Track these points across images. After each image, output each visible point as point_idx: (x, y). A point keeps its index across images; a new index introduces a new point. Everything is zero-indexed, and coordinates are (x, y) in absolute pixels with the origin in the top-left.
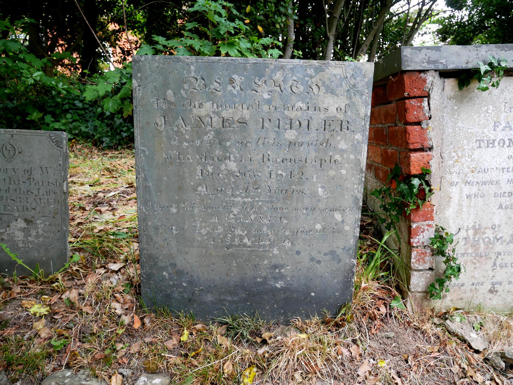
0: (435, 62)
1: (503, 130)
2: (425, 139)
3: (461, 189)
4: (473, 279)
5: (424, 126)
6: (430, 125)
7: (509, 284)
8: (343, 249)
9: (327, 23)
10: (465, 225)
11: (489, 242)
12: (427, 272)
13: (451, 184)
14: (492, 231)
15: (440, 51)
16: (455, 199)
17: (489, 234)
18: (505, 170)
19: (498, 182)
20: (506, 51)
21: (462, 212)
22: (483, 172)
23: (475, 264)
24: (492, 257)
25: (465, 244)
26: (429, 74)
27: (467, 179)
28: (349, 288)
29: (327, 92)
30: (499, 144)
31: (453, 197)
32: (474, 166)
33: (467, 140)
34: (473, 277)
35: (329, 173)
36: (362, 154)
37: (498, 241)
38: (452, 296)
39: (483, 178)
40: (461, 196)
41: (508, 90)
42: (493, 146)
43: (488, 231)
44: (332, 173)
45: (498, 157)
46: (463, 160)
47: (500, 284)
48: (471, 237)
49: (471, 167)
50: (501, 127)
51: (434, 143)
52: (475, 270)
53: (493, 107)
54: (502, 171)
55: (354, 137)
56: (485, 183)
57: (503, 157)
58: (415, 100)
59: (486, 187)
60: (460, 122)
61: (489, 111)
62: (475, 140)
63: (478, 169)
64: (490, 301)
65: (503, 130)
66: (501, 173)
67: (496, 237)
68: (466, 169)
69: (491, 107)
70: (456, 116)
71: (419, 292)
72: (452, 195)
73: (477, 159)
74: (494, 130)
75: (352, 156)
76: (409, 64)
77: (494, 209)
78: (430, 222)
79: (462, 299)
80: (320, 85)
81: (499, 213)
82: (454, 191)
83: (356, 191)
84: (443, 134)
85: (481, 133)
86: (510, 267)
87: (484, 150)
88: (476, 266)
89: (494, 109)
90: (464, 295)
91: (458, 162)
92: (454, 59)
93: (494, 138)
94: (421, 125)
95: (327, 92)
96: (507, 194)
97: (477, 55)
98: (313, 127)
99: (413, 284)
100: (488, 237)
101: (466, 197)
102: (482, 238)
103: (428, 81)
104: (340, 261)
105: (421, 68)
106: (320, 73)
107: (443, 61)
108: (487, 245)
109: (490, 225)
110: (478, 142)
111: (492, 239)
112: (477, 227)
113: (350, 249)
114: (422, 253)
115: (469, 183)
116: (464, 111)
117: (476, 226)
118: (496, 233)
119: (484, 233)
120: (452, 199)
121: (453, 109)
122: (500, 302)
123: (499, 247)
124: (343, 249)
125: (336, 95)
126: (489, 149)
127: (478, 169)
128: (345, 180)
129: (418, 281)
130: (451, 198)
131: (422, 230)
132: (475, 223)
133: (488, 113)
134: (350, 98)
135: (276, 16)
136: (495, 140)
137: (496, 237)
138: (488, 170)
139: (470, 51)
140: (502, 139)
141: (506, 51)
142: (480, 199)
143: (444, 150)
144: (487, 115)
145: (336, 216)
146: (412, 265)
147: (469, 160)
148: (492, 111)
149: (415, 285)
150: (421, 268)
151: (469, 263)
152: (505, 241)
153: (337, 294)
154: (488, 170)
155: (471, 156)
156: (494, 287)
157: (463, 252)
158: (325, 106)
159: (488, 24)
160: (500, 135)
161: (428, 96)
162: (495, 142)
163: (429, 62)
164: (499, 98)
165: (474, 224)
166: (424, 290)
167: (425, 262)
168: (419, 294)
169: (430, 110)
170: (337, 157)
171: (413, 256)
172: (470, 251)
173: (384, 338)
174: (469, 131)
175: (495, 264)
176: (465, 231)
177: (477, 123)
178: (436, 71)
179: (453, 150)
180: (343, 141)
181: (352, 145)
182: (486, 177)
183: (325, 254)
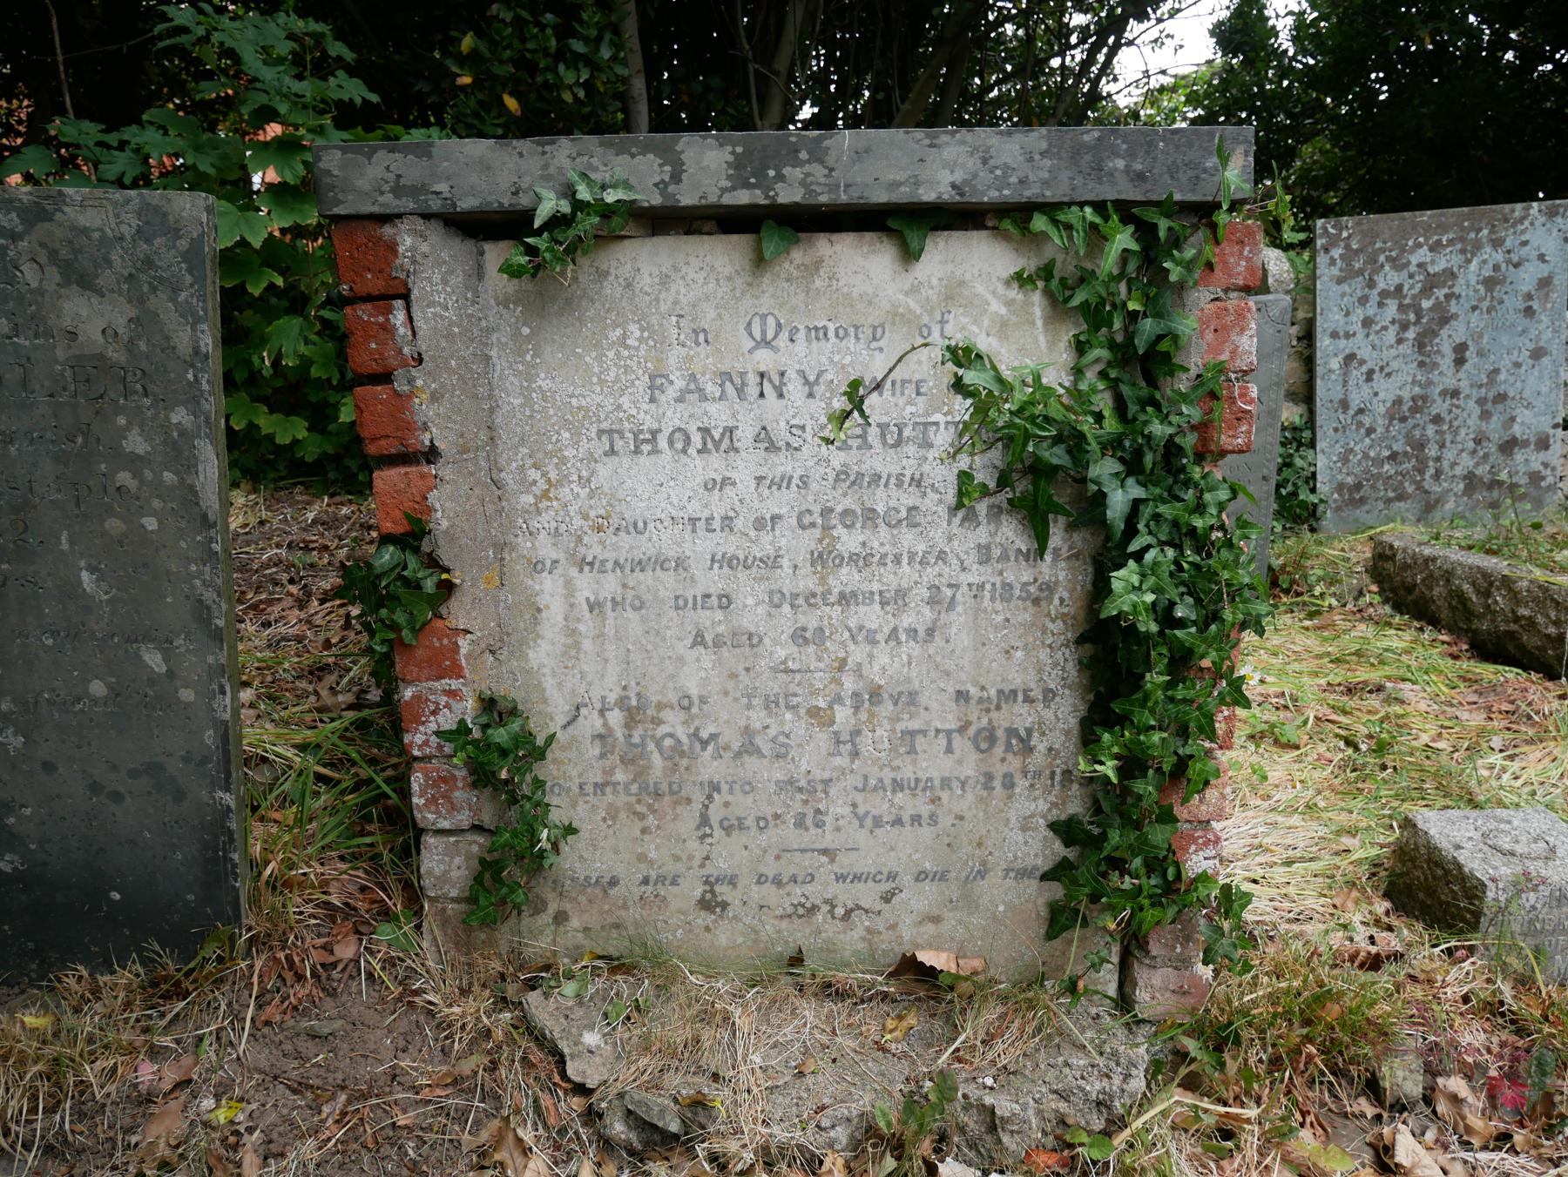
0: (416, 191)
1: (680, 400)
2: (409, 427)
3: (568, 583)
4: (643, 866)
5: (400, 386)
6: (420, 383)
7: (759, 882)
8: (186, 760)
9: (753, 90)
10: (596, 694)
11: (678, 750)
12: (470, 837)
13: (536, 566)
14: (682, 715)
15: (430, 157)
16: (555, 612)
17: (674, 723)
18: (701, 525)
19: (681, 563)
20: (633, 156)
21: (582, 656)
22: (631, 529)
23: (642, 817)
24: (694, 797)
25: (603, 756)
26: (404, 225)
27: (582, 550)
28: (227, 881)
29: (66, 282)
30: (671, 443)
31: (547, 607)
32: (602, 512)
33: (569, 430)
34: (642, 858)
35: (107, 525)
36: (201, 468)
37: (704, 749)
38: (586, 917)
39: (631, 548)
40: (572, 605)
41: (683, 278)
42: (655, 451)
43: (667, 715)
44: (114, 525)
45: (672, 483)
46: (564, 493)
47: (732, 881)
48: (619, 733)
49: (593, 514)
50: (672, 392)
51: (438, 434)
52: (647, 837)
53: (642, 330)
54: (689, 528)
55: (167, 419)
56: (640, 565)
57: (688, 484)
58: (368, 306)
59: (646, 579)
60: (542, 375)
61: (629, 342)
62: (594, 430)
63: (615, 522)
64: (709, 936)
65: (680, 400)
66: (687, 535)
67: (695, 735)
68: (578, 522)
69: (634, 329)
70: (528, 358)
71: (454, 900)
72: (541, 602)
73: (606, 490)
74: (652, 400)
75: (168, 476)
76: (340, 196)
77: (682, 648)
78: (455, 684)
79: (617, 926)
80: (43, 260)
81: (698, 660)
82: (548, 588)
83: (198, 582)
84: (492, 411)
85: (610, 408)
86: (754, 829)
87: (626, 461)
88: (646, 823)
89: (646, 334)
90: (623, 913)
91: (549, 499)
92: (474, 179)
93: (655, 426)
94: (391, 382)
95: (66, 282)
96: (714, 601)
97: (546, 167)
98: (37, 387)
99: (430, 872)
100: (671, 735)
101: (585, 607)
102: (652, 737)
103: (401, 249)
104: (180, 795)
105: (376, 209)
106: (40, 225)
107: (442, 187)
108: (670, 758)
109: (673, 697)
110: (605, 438)
111: (685, 739)
112: (634, 703)
113: (205, 760)
114: (443, 780)
115: (591, 564)
116: (554, 341)
117: (628, 698)
118: (697, 723)
119: (657, 722)
120: (544, 615)
121: (516, 334)
122: (740, 940)
123: (710, 767)
124: (186, 760)
125: (95, 291)
126: (642, 460)
127: (615, 522)
128: (157, 549)
129: (444, 865)
130: (539, 610)
131: (432, 707)
132: (625, 688)
133: (627, 347)
134: (142, 301)
135: (561, 68)
136: (660, 430)
137: (695, 735)
138: (645, 523)
139: (521, 155)
140: (680, 429)
141: (633, 156)
142: (630, 614)
143: (502, 462)
144: (626, 353)
145: (147, 657)
146: (418, 816)
147: (584, 493)
148: (640, 340)
149: (437, 878)
150: (445, 824)
151: (623, 815)
152: (727, 748)
153: (190, 897)
154: (645, 523)
155: (589, 481)
156: (712, 892)
157: (600, 780)
158: (67, 323)
159: (1377, 80)
160: (673, 417)
161: (406, 297)
162: (659, 437)
163: (398, 191)
164: (657, 300)
165: (623, 693)
166: (467, 894)
167: (454, 808)
168: (456, 906)
169: (414, 334)
170: (124, 478)
171: (415, 787)
172: (620, 776)
173: (303, 1037)
174: (574, 401)
175: (704, 820)
176: (595, 713)
177: (595, 380)
178: (427, 217)
179: (529, 462)
180: (136, 431)
181: (165, 442)
182: (645, 546)
183: (133, 774)
